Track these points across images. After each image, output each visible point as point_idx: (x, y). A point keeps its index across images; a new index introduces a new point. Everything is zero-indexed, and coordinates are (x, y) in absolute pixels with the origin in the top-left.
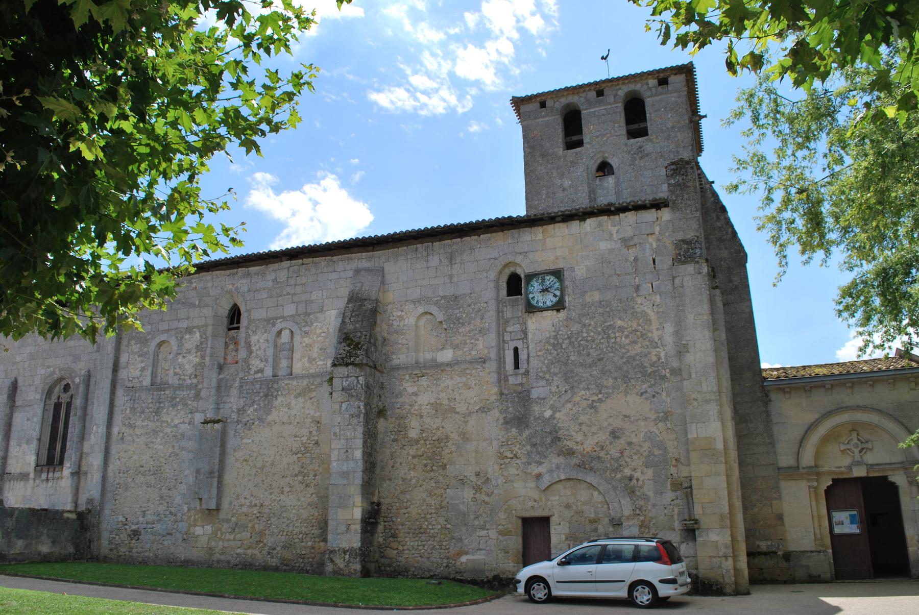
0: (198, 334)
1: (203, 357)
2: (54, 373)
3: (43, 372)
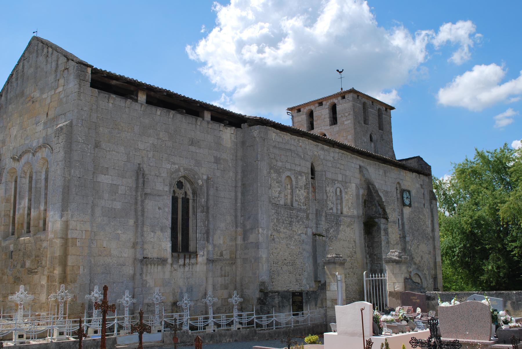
0: (304, 178)
1: (308, 193)
2: (178, 170)
3: (168, 166)
